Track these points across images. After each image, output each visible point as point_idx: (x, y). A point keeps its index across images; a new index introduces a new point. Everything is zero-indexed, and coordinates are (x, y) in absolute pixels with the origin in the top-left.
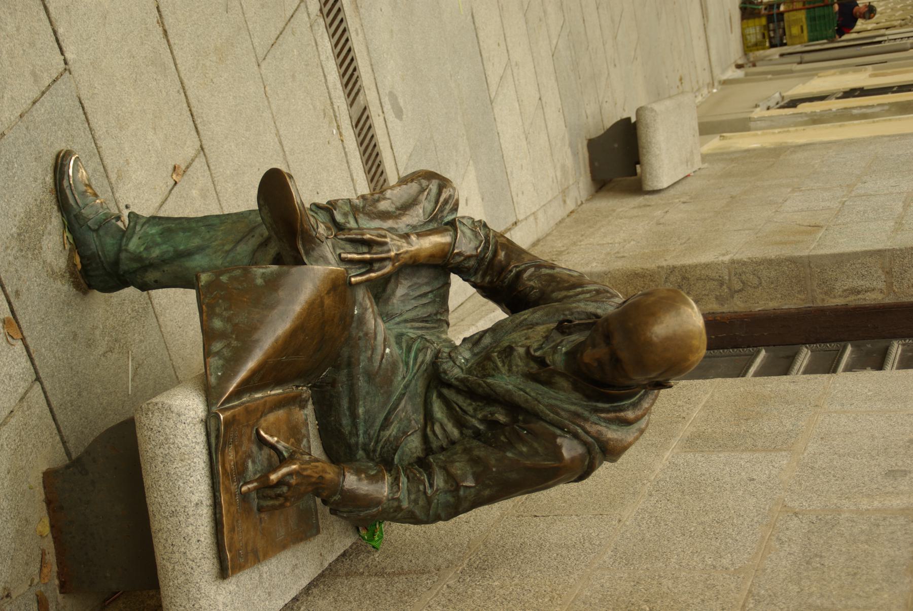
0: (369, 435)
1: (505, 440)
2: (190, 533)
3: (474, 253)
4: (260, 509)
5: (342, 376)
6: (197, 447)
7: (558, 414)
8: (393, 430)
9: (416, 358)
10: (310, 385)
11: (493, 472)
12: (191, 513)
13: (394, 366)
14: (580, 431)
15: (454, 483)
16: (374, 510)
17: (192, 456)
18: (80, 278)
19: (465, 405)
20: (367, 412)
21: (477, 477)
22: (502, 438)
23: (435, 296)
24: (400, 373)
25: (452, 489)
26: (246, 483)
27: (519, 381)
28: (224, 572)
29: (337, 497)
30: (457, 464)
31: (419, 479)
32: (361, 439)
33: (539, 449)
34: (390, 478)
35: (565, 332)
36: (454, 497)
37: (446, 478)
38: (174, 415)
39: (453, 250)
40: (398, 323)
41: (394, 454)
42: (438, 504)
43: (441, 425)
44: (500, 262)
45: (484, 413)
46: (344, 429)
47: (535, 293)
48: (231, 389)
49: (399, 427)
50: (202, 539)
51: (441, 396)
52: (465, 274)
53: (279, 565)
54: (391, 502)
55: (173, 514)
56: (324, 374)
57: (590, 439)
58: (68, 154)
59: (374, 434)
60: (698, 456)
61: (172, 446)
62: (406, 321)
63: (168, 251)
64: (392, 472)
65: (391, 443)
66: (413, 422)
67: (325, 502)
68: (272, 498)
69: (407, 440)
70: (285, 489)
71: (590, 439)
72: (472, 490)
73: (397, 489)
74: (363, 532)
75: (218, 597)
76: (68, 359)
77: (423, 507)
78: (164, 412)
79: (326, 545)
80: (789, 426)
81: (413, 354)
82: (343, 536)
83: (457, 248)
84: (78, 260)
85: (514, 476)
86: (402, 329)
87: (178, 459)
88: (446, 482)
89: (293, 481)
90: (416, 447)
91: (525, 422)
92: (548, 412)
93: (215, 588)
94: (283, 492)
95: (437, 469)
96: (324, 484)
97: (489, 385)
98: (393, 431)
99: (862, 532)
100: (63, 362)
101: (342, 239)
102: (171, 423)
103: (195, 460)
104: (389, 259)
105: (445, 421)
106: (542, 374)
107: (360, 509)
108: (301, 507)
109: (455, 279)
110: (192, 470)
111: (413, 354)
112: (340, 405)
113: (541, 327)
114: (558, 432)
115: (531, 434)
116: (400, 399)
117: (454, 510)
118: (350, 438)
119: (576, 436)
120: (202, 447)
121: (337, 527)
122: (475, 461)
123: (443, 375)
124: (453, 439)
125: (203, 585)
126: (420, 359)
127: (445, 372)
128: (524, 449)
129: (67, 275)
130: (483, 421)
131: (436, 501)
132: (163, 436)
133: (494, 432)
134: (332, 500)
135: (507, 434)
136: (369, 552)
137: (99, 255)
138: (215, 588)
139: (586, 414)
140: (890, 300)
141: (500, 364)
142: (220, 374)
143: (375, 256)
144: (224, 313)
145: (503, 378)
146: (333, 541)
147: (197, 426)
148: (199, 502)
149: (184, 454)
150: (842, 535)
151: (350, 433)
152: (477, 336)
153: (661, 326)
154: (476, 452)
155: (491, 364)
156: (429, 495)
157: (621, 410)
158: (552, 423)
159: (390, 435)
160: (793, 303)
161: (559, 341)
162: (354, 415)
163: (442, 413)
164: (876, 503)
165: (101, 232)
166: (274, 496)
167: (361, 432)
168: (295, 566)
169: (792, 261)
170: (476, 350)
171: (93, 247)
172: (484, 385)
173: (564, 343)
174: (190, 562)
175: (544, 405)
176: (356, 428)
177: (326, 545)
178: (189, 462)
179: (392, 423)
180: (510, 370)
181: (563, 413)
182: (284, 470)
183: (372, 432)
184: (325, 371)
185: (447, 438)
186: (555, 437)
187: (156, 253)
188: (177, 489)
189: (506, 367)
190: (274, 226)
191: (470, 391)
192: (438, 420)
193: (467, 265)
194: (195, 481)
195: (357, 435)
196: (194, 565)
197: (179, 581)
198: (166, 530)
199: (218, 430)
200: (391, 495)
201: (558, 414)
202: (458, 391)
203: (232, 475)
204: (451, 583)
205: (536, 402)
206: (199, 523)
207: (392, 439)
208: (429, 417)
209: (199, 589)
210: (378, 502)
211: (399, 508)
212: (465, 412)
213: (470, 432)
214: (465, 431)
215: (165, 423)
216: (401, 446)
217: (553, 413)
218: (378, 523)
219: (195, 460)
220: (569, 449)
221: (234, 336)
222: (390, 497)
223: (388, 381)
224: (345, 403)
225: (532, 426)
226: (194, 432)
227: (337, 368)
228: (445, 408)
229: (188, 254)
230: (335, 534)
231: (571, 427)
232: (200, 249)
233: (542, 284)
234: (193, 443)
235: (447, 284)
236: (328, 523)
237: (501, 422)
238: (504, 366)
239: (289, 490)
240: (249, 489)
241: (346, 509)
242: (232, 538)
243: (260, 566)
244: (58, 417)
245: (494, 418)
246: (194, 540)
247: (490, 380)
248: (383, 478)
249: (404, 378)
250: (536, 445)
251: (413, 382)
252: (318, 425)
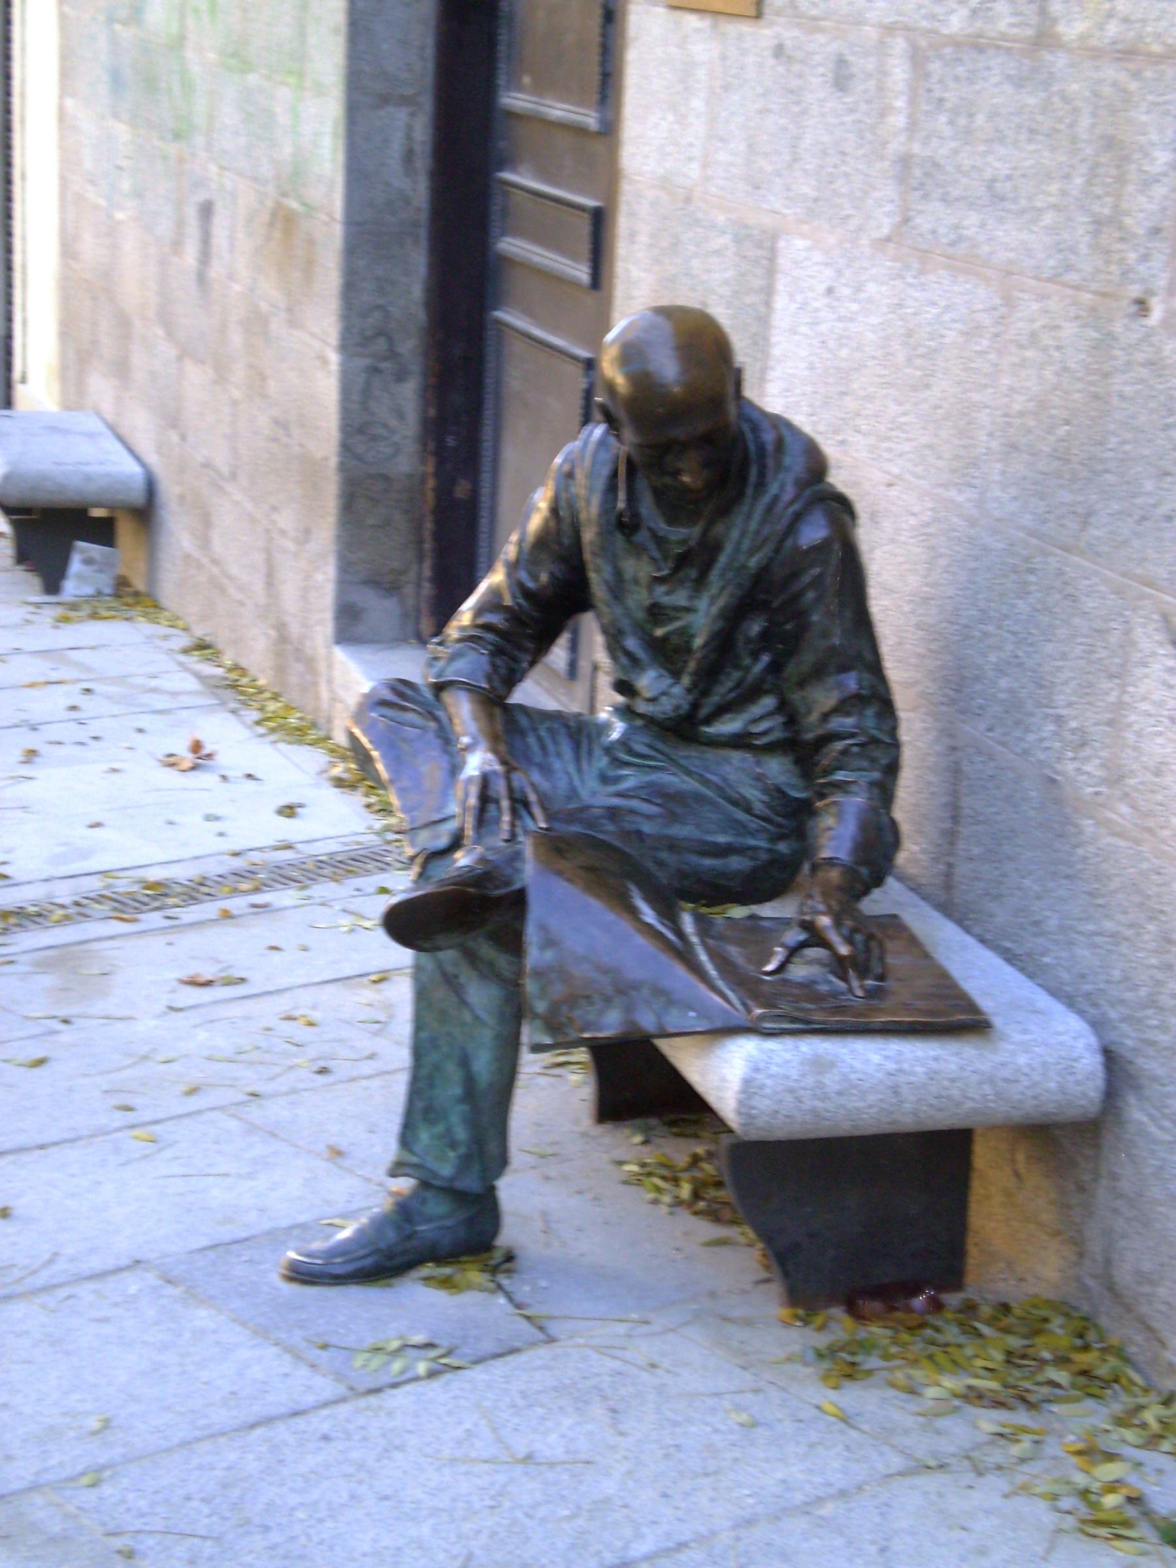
22: (788, 627)
32: (762, 843)
40: (582, 781)
41: (789, 796)
47: (558, 570)
51: (709, 720)
52: (512, 680)
55: (895, 1091)
60: (771, 375)
80: (725, 240)
85: (848, 614)
99: (951, 123)
116: (706, 782)
119: (798, 517)
122: (818, 673)
127: (678, 708)
130: (755, 656)
140: (427, 103)
150: (956, 152)
157: (761, 448)
158: (777, 550)
160: (418, 260)
164: (900, 103)
169: (351, 250)
186: (796, 549)
187: (461, 1133)
191: (708, 676)
192: (746, 725)
202: (705, 693)
204: (982, 726)
208: (740, 742)
213: (770, 678)
220: (813, 532)
229: (469, 1081)
232: (465, 1062)
246: (934, 1065)
247: (698, 642)
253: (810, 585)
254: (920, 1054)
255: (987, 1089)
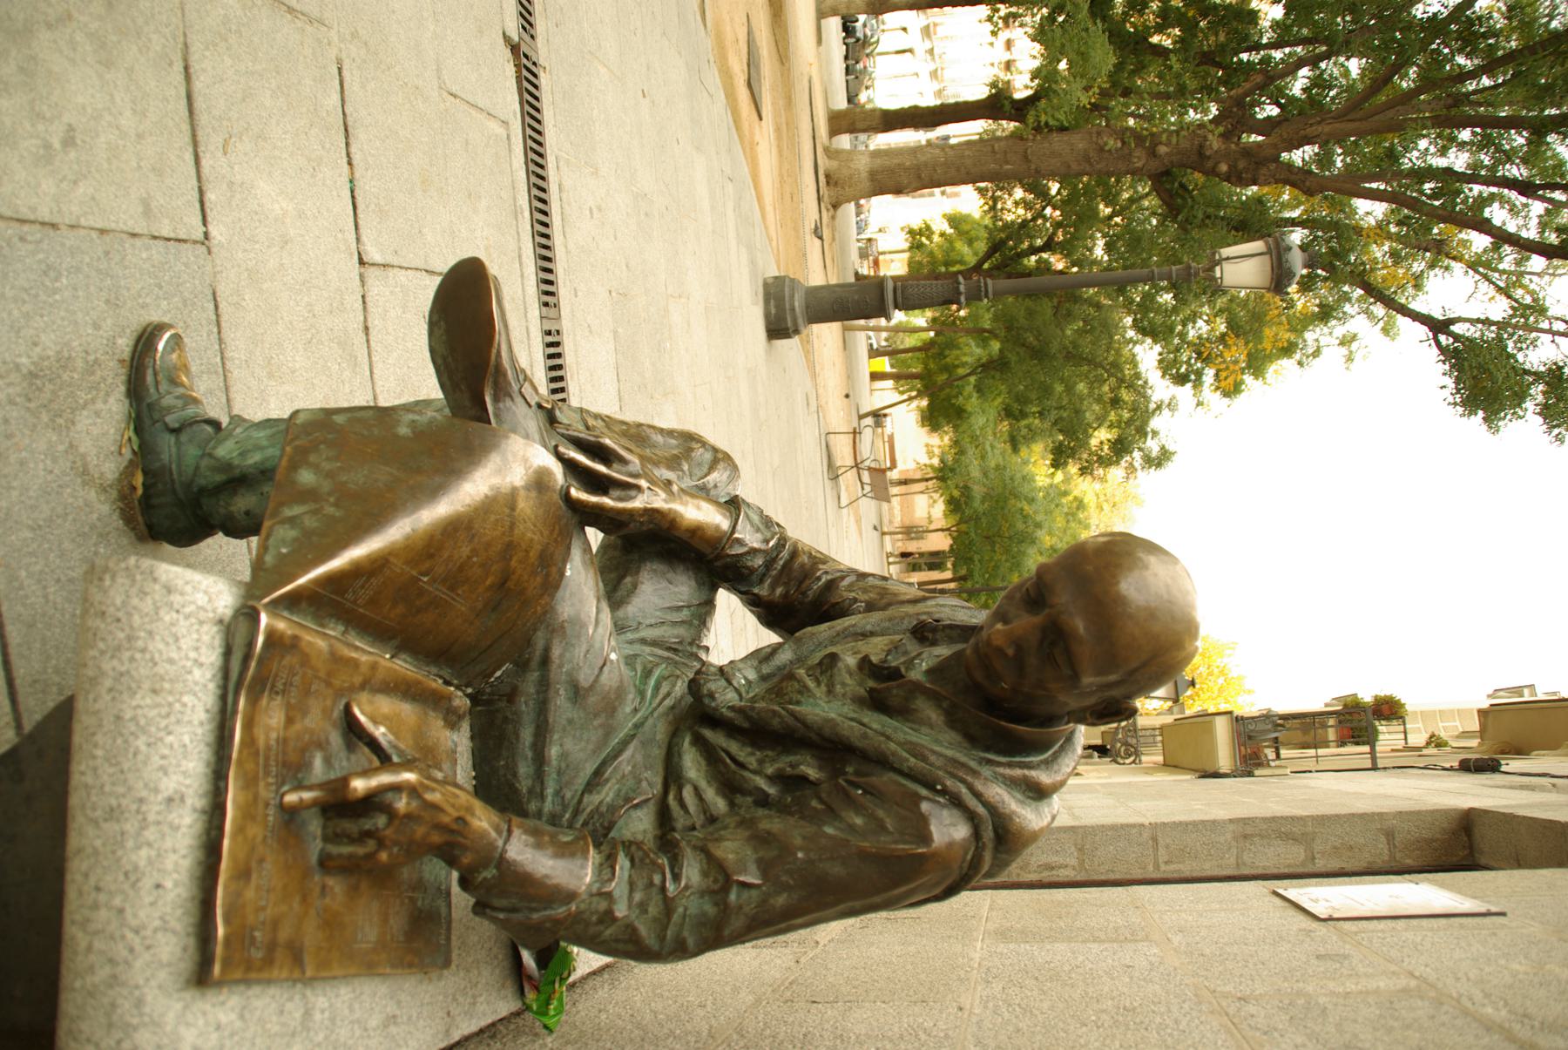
0: (563, 798)
1: (819, 806)
2: (142, 863)
3: (763, 547)
4: (325, 863)
5: (529, 684)
6: (197, 673)
7: (924, 759)
8: (606, 794)
9: (657, 688)
10: (469, 690)
11: (797, 859)
12: (152, 817)
13: (620, 692)
14: (964, 790)
15: (721, 878)
16: (560, 910)
17: (179, 686)
18: (137, 509)
19: (742, 754)
20: (564, 756)
21: (765, 867)
22: (814, 803)
24: (629, 702)
25: (716, 887)
26: (300, 787)
27: (848, 709)
28: (202, 976)
29: (489, 873)
30: (727, 844)
31: (654, 863)
34: (597, 856)
35: (927, 639)
36: (716, 904)
37: (705, 866)
38: (157, 587)
40: (631, 642)
42: (684, 916)
43: (696, 789)
44: (803, 565)
45: (777, 766)
46: (519, 782)
48: (302, 581)
49: (620, 790)
50: (169, 884)
51: (699, 741)
53: (357, 1006)
54: (595, 899)
56: (498, 674)
57: (981, 810)
58: (159, 328)
59: (573, 797)
61: (138, 656)
62: (643, 641)
64: (602, 848)
65: (602, 815)
66: (644, 784)
67: (464, 883)
68: (352, 840)
69: (630, 816)
70: (381, 821)
71: (981, 810)
72: (754, 893)
73: (610, 875)
74: (531, 996)
75: (183, 1030)
76: (74, 615)
77: (655, 920)
78: (138, 577)
79: (461, 999)
81: (652, 682)
82: (494, 994)
84: (139, 480)
85: (836, 870)
86: (637, 648)
87: (146, 685)
88: (705, 874)
89: (402, 804)
90: (645, 831)
91: (857, 773)
92: (905, 754)
93: (179, 1006)
94: (377, 829)
95: (688, 850)
96: (465, 838)
97: (792, 714)
98: (607, 794)
100: (63, 615)
101: (563, 435)
102: (147, 605)
103: (186, 699)
105: (703, 784)
106: (895, 691)
107: (534, 905)
108: (419, 903)
109: (726, 600)
110: (173, 719)
111: (652, 682)
112: (517, 736)
113: (880, 638)
114: (924, 792)
115: (872, 794)
116: (624, 744)
117: (715, 935)
118: (529, 801)
119: (956, 802)
120: (209, 675)
121: (485, 973)
122: (761, 840)
123: (706, 701)
124: (714, 813)
125: (151, 995)
126: (664, 690)
128: (859, 821)
129: (114, 494)
130: (772, 779)
131: (681, 910)
132: (123, 630)
133: (798, 793)
134: (480, 879)
135: (823, 795)
136: (536, 1035)
137: (170, 470)
138: (179, 1006)
139: (973, 764)
141: (811, 684)
142: (284, 551)
143: (615, 475)
144: (324, 464)
145: (817, 705)
146: (474, 997)
147: (205, 628)
148: (177, 797)
149: (162, 679)
151: (530, 791)
152: (769, 650)
154: (765, 825)
155: (796, 684)
156: (670, 894)
159: (601, 803)
161: (915, 654)
162: (540, 759)
163: (698, 770)
165: (184, 437)
166: (356, 836)
167: (549, 791)
168: (392, 1019)
170: (766, 669)
171: (165, 457)
172: (783, 712)
173: (924, 656)
174: (130, 935)
175: (899, 744)
176: (542, 783)
177: (461, 999)
178: (171, 699)
179: (607, 780)
180: (830, 692)
181: (933, 758)
182: (385, 778)
183: (568, 795)
184: (499, 668)
185: (705, 813)
186: (918, 798)
188: (130, 756)
189: (823, 688)
190: (450, 359)
192: (689, 781)
193: (749, 564)
194: (176, 746)
195: (542, 797)
196: (136, 941)
197: (96, 979)
198: (89, 850)
199: (251, 644)
200: (597, 885)
201: (924, 759)
203: (267, 758)
205: (882, 739)
206: (168, 844)
207: (603, 809)
208: (672, 776)
209: (139, 1003)
210: (571, 896)
211: (608, 917)
212: (742, 765)
214: (739, 799)
215: (135, 601)
216: (617, 826)
217: (915, 756)
218: (558, 979)
219: (186, 699)
220: (948, 830)
221: (332, 500)
222: (594, 890)
223: (610, 707)
224: (527, 735)
225: (874, 780)
226: (195, 636)
227: (522, 666)
228: (703, 763)
230: (479, 986)
231: (948, 783)
234: (187, 658)
235: (709, 604)
236: (470, 960)
237: (811, 778)
238: (819, 683)
239: (389, 824)
240: (301, 800)
241: (503, 903)
242: (239, 894)
243: (308, 992)
244: (21, 698)
245: (796, 772)
246: (147, 883)
248: (585, 853)
249: (636, 710)
250: (881, 813)
251: (650, 721)
252: (475, 778)
253: (872, 817)
254: (170, 861)
255: (103, 973)
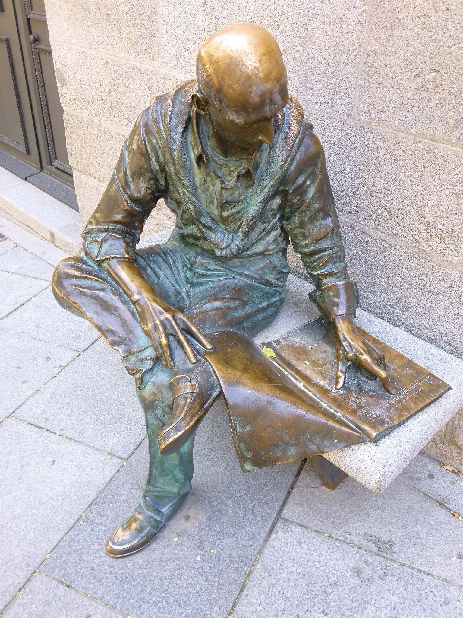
23: (150, 261)
33: (127, 159)
39: (126, 258)
63: (180, 469)
81: (209, 273)
83: (124, 256)
104: (174, 317)
111: (209, 273)
153: (246, 60)
159: (275, 279)
233: (143, 181)
